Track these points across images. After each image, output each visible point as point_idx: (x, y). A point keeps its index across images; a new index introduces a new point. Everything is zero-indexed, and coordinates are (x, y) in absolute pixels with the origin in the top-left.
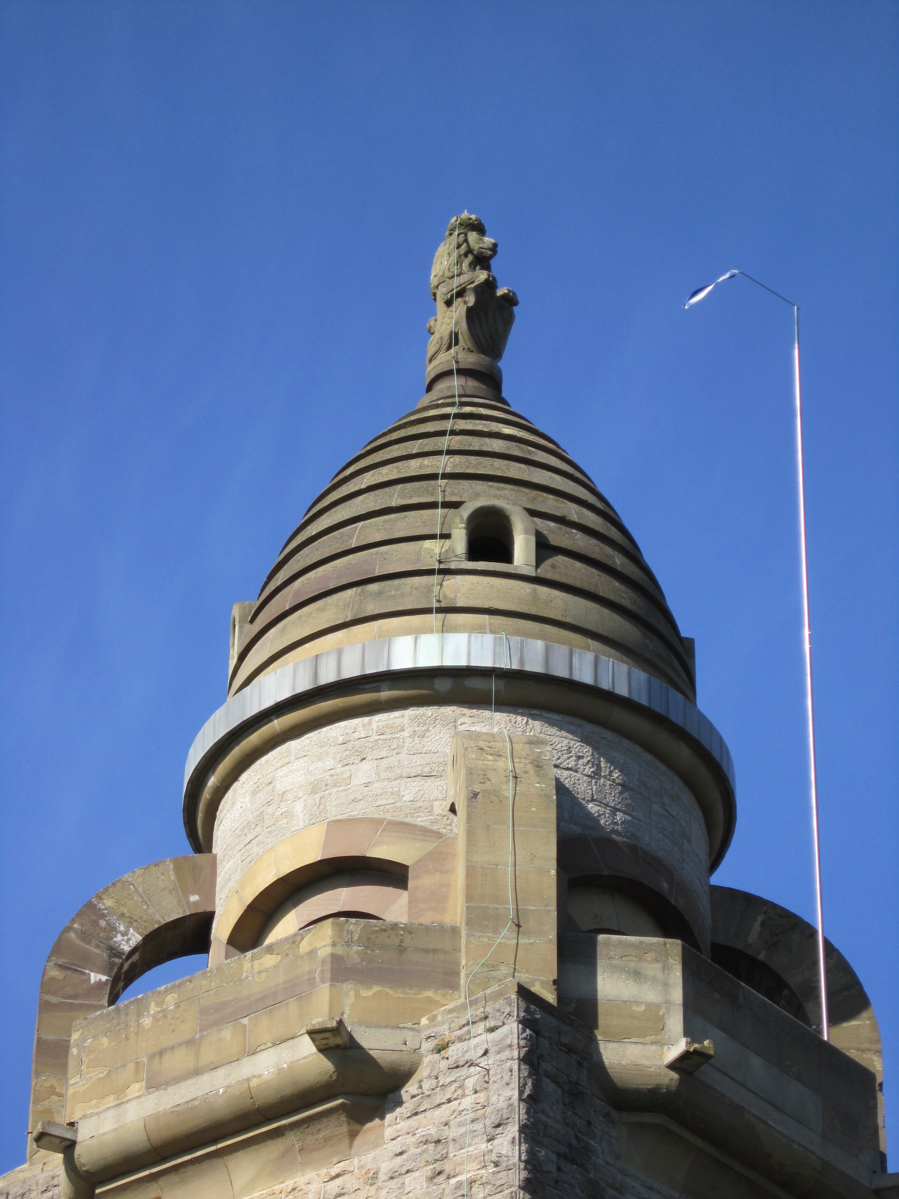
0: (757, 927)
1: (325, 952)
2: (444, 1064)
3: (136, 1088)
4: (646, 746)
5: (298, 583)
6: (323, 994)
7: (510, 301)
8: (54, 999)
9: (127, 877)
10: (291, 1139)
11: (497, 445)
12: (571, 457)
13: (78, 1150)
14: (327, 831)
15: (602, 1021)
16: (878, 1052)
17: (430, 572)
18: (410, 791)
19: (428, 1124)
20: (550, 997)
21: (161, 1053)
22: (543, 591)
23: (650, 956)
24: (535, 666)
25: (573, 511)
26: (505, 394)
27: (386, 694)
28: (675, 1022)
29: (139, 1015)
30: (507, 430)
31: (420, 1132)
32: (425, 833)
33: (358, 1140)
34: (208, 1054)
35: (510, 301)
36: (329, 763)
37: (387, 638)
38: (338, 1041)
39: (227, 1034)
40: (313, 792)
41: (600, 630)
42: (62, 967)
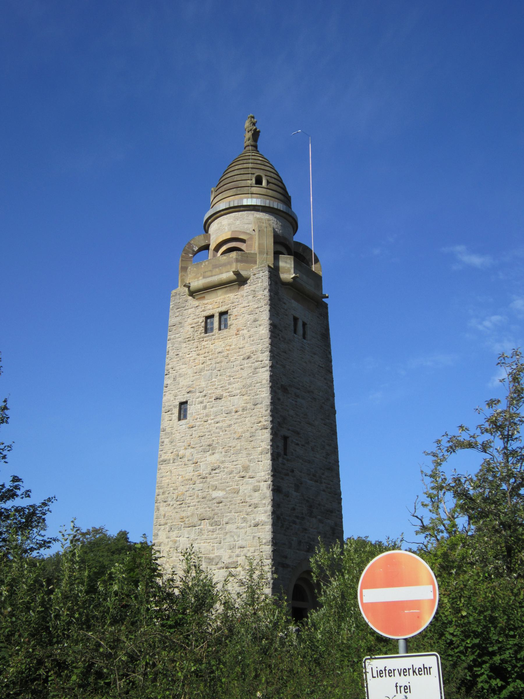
0: (301, 248)
1: (235, 257)
2: (255, 278)
3: (201, 278)
4: (285, 218)
5: (225, 186)
6: (234, 265)
7: (259, 132)
8: (184, 259)
9: (195, 237)
10: (228, 288)
11: (259, 162)
12: (271, 163)
13: (191, 288)
14: (232, 233)
15: (280, 270)
16: (321, 271)
17: (249, 186)
18: (246, 226)
19: (252, 287)
20: (272, 266)
21: (205, 272)
22: (268, 190)
23: (288, 259)
24: (267, 205)
25: (272, 175)
26: (258, 149)
27: (242, 209)
28: (292, 271)
29: (201, 265)
30: (261, 159)
31: (251, 289)
32: (249, 234)
33: (240, 289)
34: (214, 273)
35: (259, 132)
36: (232, 220)
37: (242, 199)
38: (238, 273)
39: (217, 270)
40: (229, 225)
41: (278, 198)
42: (185, 253)
